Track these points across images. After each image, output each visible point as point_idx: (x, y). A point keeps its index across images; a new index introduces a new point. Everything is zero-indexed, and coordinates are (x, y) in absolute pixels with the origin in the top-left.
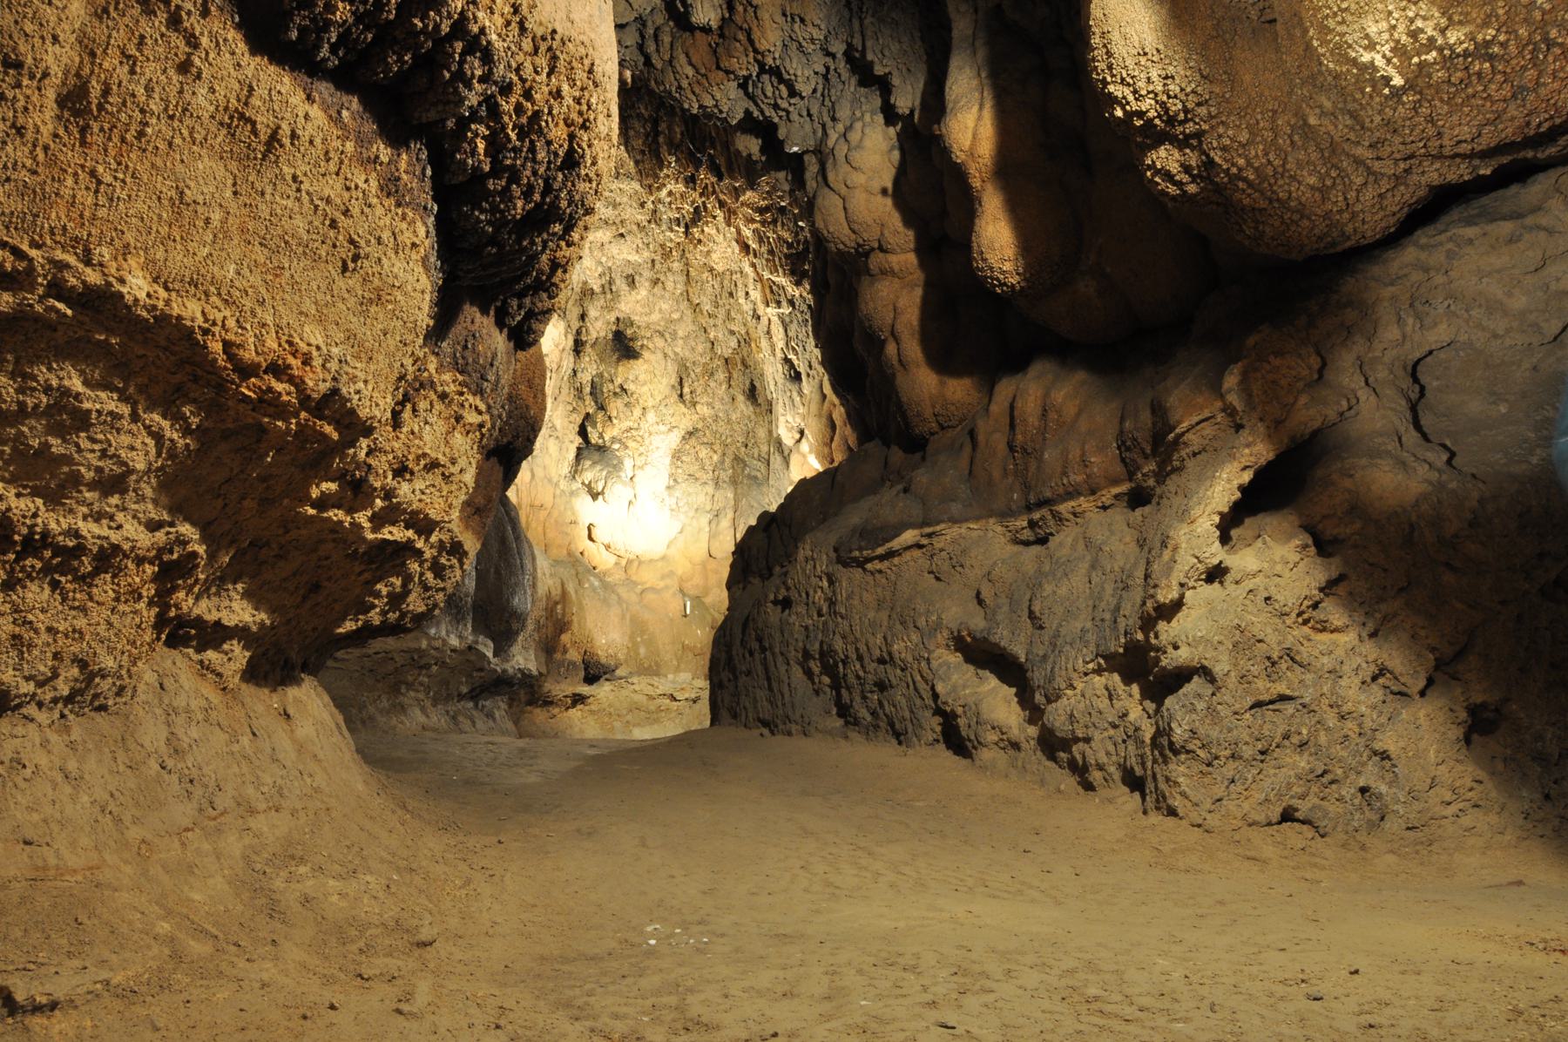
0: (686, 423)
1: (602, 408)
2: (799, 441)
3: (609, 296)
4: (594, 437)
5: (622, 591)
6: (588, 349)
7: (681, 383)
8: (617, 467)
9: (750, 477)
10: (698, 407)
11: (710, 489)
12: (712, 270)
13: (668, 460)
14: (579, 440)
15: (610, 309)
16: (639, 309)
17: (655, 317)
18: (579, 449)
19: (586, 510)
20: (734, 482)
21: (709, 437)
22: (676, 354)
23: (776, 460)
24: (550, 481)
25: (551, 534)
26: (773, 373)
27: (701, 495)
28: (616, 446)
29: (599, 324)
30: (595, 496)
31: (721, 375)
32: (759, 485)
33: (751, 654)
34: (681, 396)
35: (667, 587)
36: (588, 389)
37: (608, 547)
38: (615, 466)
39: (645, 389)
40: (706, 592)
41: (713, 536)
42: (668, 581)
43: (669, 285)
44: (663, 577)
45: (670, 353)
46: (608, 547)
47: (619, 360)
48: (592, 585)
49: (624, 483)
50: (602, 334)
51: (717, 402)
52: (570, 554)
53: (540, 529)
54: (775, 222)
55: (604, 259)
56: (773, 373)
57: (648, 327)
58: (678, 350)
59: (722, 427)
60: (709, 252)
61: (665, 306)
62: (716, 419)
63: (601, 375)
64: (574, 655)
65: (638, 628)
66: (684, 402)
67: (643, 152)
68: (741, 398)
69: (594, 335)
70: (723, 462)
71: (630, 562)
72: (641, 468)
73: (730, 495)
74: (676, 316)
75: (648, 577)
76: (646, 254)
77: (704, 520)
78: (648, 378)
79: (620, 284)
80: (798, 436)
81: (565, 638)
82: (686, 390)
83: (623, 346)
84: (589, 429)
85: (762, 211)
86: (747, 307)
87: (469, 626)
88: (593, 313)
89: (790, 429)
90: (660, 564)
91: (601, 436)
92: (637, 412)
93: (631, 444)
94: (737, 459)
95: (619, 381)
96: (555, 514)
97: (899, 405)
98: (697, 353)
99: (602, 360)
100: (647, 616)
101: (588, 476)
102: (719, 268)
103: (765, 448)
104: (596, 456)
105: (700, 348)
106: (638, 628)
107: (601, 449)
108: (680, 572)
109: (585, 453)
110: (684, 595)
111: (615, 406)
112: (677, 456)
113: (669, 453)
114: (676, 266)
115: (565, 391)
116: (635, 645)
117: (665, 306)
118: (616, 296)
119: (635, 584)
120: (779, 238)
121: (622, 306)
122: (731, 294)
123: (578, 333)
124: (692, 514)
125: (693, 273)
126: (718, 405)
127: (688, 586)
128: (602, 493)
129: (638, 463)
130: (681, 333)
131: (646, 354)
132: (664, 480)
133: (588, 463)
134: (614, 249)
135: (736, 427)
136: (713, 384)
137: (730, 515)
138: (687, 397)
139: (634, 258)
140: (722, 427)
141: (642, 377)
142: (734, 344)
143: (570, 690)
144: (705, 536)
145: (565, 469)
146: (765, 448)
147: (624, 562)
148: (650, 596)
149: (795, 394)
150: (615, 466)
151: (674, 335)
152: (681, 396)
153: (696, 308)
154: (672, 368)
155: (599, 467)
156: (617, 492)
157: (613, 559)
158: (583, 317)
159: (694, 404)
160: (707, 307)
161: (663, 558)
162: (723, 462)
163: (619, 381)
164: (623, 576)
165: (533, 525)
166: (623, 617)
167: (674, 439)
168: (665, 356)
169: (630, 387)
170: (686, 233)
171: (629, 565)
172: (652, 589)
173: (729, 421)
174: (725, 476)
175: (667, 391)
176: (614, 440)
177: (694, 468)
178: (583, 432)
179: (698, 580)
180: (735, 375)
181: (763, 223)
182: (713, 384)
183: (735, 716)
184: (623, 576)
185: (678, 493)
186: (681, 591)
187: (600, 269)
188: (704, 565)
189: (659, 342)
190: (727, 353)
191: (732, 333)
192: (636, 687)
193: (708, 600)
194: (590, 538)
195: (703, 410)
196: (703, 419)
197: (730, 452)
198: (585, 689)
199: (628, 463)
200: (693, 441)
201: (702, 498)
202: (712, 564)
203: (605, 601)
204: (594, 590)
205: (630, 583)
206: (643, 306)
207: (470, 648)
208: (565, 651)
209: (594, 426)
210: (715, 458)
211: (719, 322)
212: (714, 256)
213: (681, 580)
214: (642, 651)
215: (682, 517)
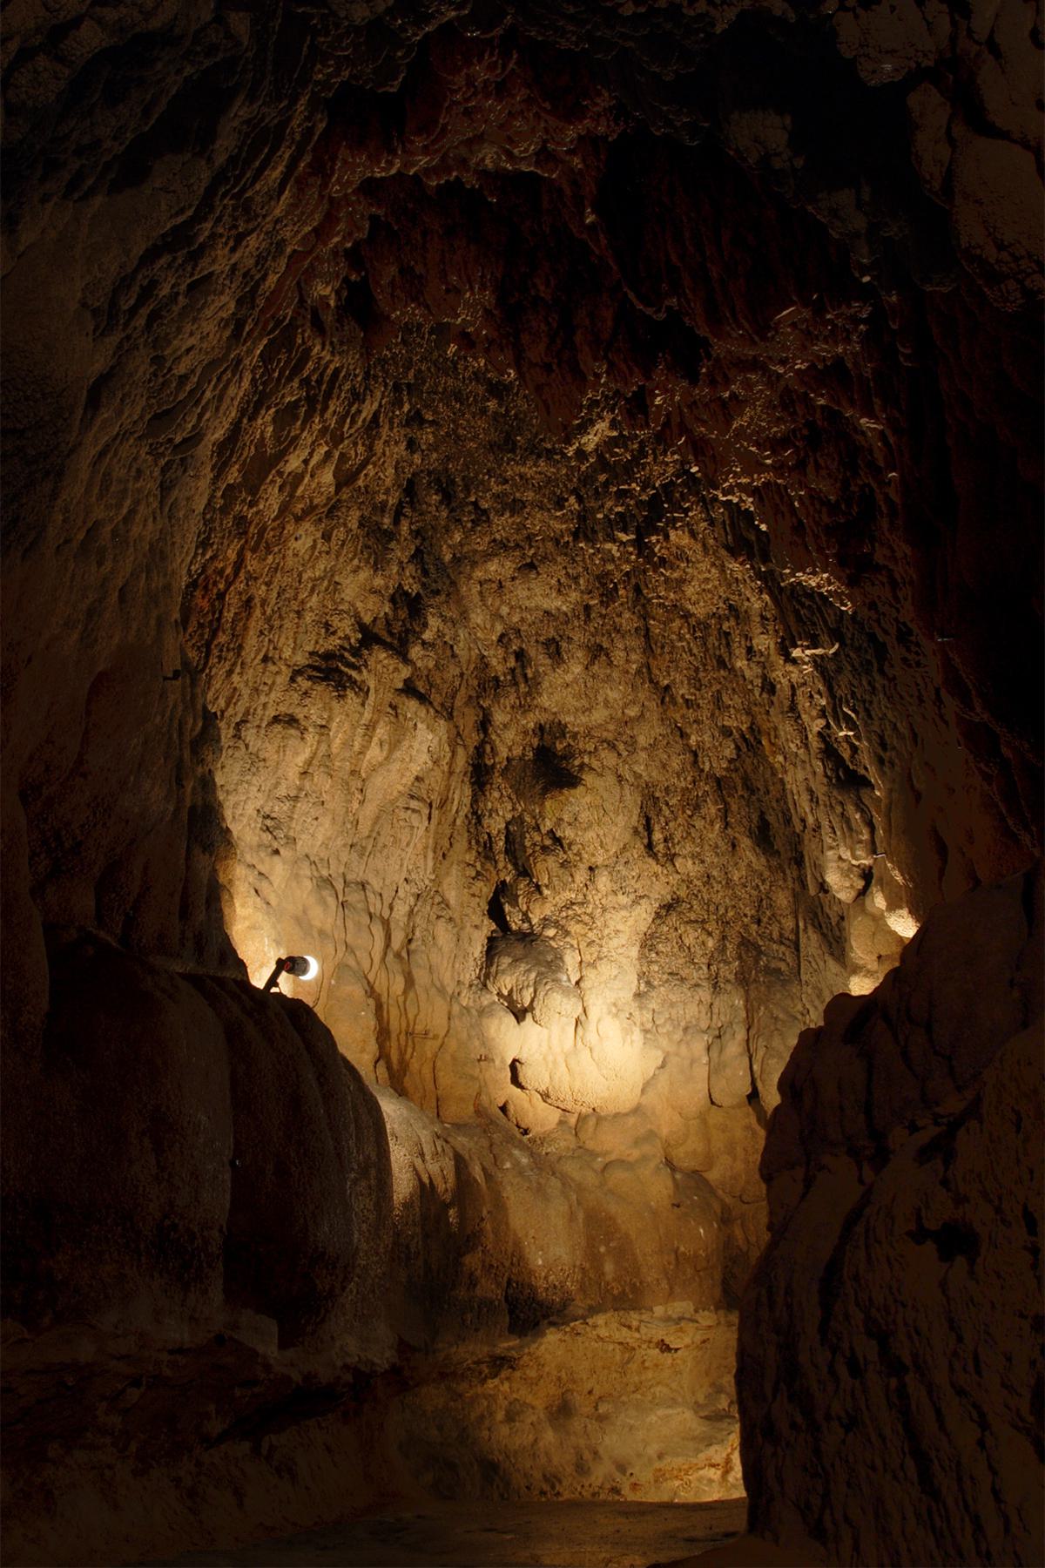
0: (661, 891)
1: (524, 872)
2: (863, 893)
3: (523, 688)
4: (515, 921)
5: (570, 1168)
6: (498, 779)
7: (649, 828)
8: (550, 966)
9: (768, 971)
10: (678, 862)
11: (705, 994)
12: (687, 616)
13: (634, 952)
14: (489, 926)
15: (524, 708)
16: (572, 702)
17: (599, 715)
18: (491, 940)
19: (512, 1039)
20: (743, 980)
21: (698, 911)
22: (638, 776)
23: (811, 942)
24: (441, 991)
25: (445, 1079)
26: (801, 776)
27: (690, 1005)
28: (551, 932)
29: (510, 735)
30: (520, 1014)
31: (711, 809)
32: (784, 983)
33: (855, 1369)
34: (650, 846)
35: (644, 1159)
36: (501, 844)
37: (545, 1096)
38: (549, 964)
39: (591, 834)
40: (709, 1160)
41: (714, 1070)
42: (647, 1149)
43: (619, 656)
44: (637, 1142)
45: (628, 775)
46: (545, 1096)
47: (545, 791)
48: (516, 1163)
49: (566, 992)
50: (517, 751)
51: (707, 852)
52: (479, 1112)
53: (427, 1071)
54: (801, 466)
55: (505, 610)
56: (801, 776)
57: (589, 735)
58: (640, 769)
59: (719, 895)
60: (682, 581)
61: (613, 695)
62: (708, 879)
63: (519, 821)
64: (489, 1289)
65: (598, 1228)
66: (654, 856)
67: (547, 368)
68: (745, 842)
69: (504, 753)
70: (723, 950)
71: (582, 1119)
72: (593, 965)
73: (739, 1002)
74: (632, 712)
75: (613, 1143)
76: (574, 596)
77: (699, 1046)
78: (596, 817)
79: (540, 658)
80: (860, 884)
81: (472, 1261)
82: (657, 836)
83: (552, 768)
84: (507, 908)
85: (776, 445)
86: (750, 671)
87: (217, 1295)
88: (499, 717)
89: (846, 874)
90: (631, 1120)
91: (526, 918)
92: (581, 876)
93: (574, 928)
94: (745, 943)
95: (548, 825)
96: (452, 1044)
97: (507, 1224)
98: (670, 772)
99: (520, 794)
100: (613, 1208)
101: (506, 982)
102: (700, 611)
103: (789, 924)
104: (519, 950)
105: (676, 764)
106: (598, 1228)
107: (528, 938)
108: (665, 1131)
109: (502, 945)
110: (673, 1169)
111: (546, 868)
112: (648, 943)
113: (637, 939)
114: (628, 620)
115: (461, 843)
116: (594, 1258)
117: (613, 695)
118: (534, 685)
119: (593, 1154)
120: (814, 496)
121: (544, 700)
122: (722, 663)
123: (479, 751)
124: (678, 1035)
125: (656, 628)
126: (709, 857)
127: (679, 1154)
128: (531, 1008)
129: (587, 958)
130: (642, 741)
131: (588, 778)
132: (631, 982)
133: (506, 961)
134: (520, 592)
135: (741, 893)
136: (699, 823)
137: (741, 1034)
138: (660, 848)
139: (555, 603)
140: (719, 895)
141: (584, 816)
142: (729, 751)
143: (483, 1351)
144: (701, 1072)
145: (470, 973)
146: (789, 924)
147: (573, 1120)
148: (618, 1176)
149: (850, 808)
150: (549, 964)
151: (632, 744)
152: (650, 846)
153: (665, 694)
154: (632, 799)
155: (523, 967)
156: (558, 1007)
157: (555, 1116)
158: (484, 724)
159: (671, 858)
160: (683, 690)
161: (637, 1110)
162: (723, 950)
163: (548, 825)
164: (571, 1142)
165: (414, 1065)
166: (572, 1217)
167: (643, 916)
168: (620, 779)
169: (567, 833)
170: (640, 544)
171: (583, 1122)
172: (621, 1162)
173: (729, 883)
174: (728, 971)
175: (627, 836)
176: (546, 922)
177: (678, 962)
178: (495, 911)
179: (694, 1144)
180: (734, 807)
181: (778, 468)
182: (699, 823)
183: (818, 1532)
184: (571, 1142)
185: (653, 1005)
186: (669, 1163)
187: (499, 628)
188: (703, 1118)
189: (609, 758)
190: (720, 767)
191: (726, 732)
192: (603, 1332)
193: (713, 1176)
194: (515, 1080)
195: (687, 866)
196: (688, 882)
197: (733, 932)
198: (507, 1345)
199: (571, 959)
200: (673, 919)
201: (692, 1010)
202: (716, 1117)
203: (540, 1190)
204: (520, 1171)
205: (584, 1154)
206: (578, 697)
207: (220, 1339)
208: (473, 1284)
209: (514, 902)
210: (711, 943)
211: (704, 715)
212: (690, 590)
213: (667, 1145)
214: (609, 1267)
215: (664, 1042)
